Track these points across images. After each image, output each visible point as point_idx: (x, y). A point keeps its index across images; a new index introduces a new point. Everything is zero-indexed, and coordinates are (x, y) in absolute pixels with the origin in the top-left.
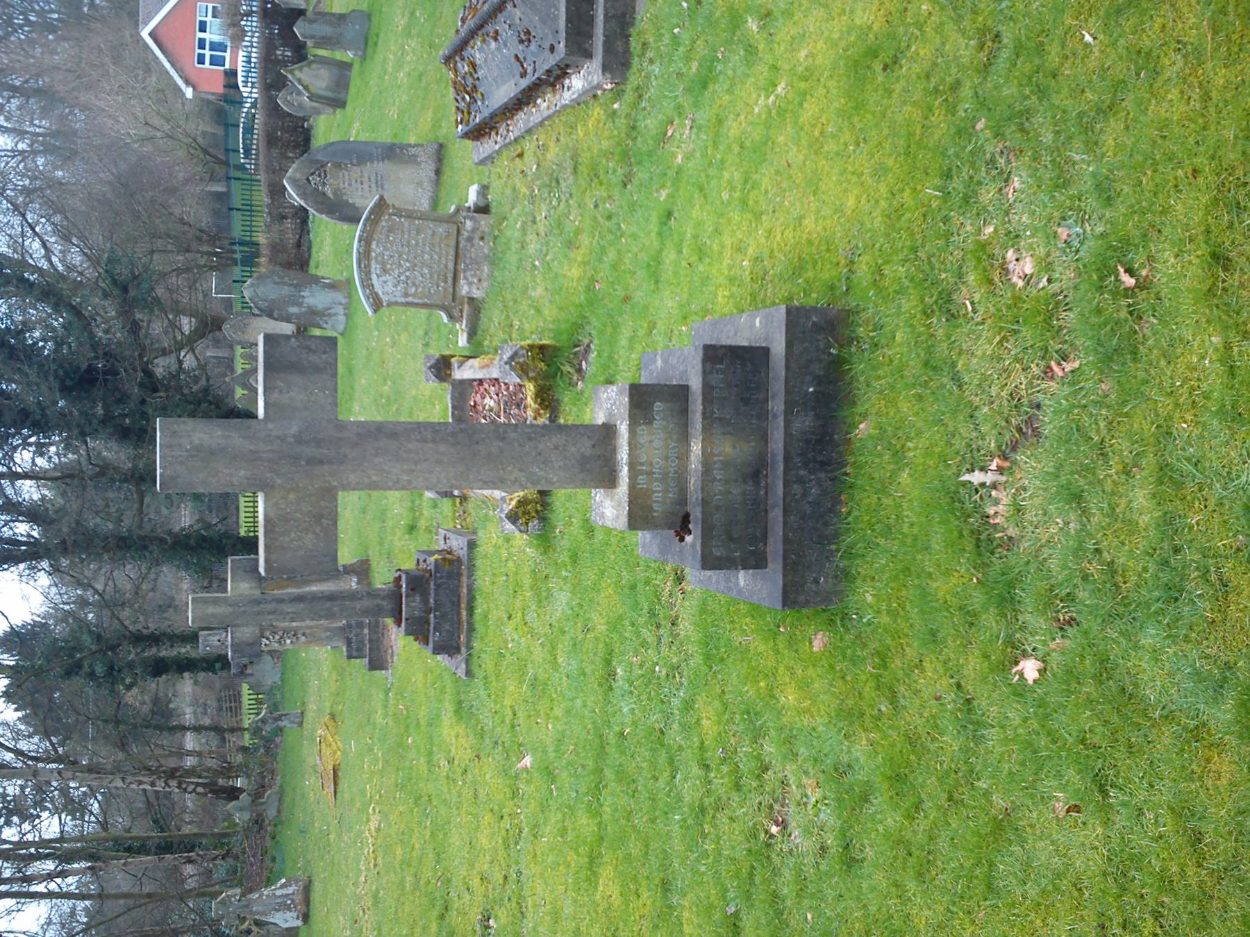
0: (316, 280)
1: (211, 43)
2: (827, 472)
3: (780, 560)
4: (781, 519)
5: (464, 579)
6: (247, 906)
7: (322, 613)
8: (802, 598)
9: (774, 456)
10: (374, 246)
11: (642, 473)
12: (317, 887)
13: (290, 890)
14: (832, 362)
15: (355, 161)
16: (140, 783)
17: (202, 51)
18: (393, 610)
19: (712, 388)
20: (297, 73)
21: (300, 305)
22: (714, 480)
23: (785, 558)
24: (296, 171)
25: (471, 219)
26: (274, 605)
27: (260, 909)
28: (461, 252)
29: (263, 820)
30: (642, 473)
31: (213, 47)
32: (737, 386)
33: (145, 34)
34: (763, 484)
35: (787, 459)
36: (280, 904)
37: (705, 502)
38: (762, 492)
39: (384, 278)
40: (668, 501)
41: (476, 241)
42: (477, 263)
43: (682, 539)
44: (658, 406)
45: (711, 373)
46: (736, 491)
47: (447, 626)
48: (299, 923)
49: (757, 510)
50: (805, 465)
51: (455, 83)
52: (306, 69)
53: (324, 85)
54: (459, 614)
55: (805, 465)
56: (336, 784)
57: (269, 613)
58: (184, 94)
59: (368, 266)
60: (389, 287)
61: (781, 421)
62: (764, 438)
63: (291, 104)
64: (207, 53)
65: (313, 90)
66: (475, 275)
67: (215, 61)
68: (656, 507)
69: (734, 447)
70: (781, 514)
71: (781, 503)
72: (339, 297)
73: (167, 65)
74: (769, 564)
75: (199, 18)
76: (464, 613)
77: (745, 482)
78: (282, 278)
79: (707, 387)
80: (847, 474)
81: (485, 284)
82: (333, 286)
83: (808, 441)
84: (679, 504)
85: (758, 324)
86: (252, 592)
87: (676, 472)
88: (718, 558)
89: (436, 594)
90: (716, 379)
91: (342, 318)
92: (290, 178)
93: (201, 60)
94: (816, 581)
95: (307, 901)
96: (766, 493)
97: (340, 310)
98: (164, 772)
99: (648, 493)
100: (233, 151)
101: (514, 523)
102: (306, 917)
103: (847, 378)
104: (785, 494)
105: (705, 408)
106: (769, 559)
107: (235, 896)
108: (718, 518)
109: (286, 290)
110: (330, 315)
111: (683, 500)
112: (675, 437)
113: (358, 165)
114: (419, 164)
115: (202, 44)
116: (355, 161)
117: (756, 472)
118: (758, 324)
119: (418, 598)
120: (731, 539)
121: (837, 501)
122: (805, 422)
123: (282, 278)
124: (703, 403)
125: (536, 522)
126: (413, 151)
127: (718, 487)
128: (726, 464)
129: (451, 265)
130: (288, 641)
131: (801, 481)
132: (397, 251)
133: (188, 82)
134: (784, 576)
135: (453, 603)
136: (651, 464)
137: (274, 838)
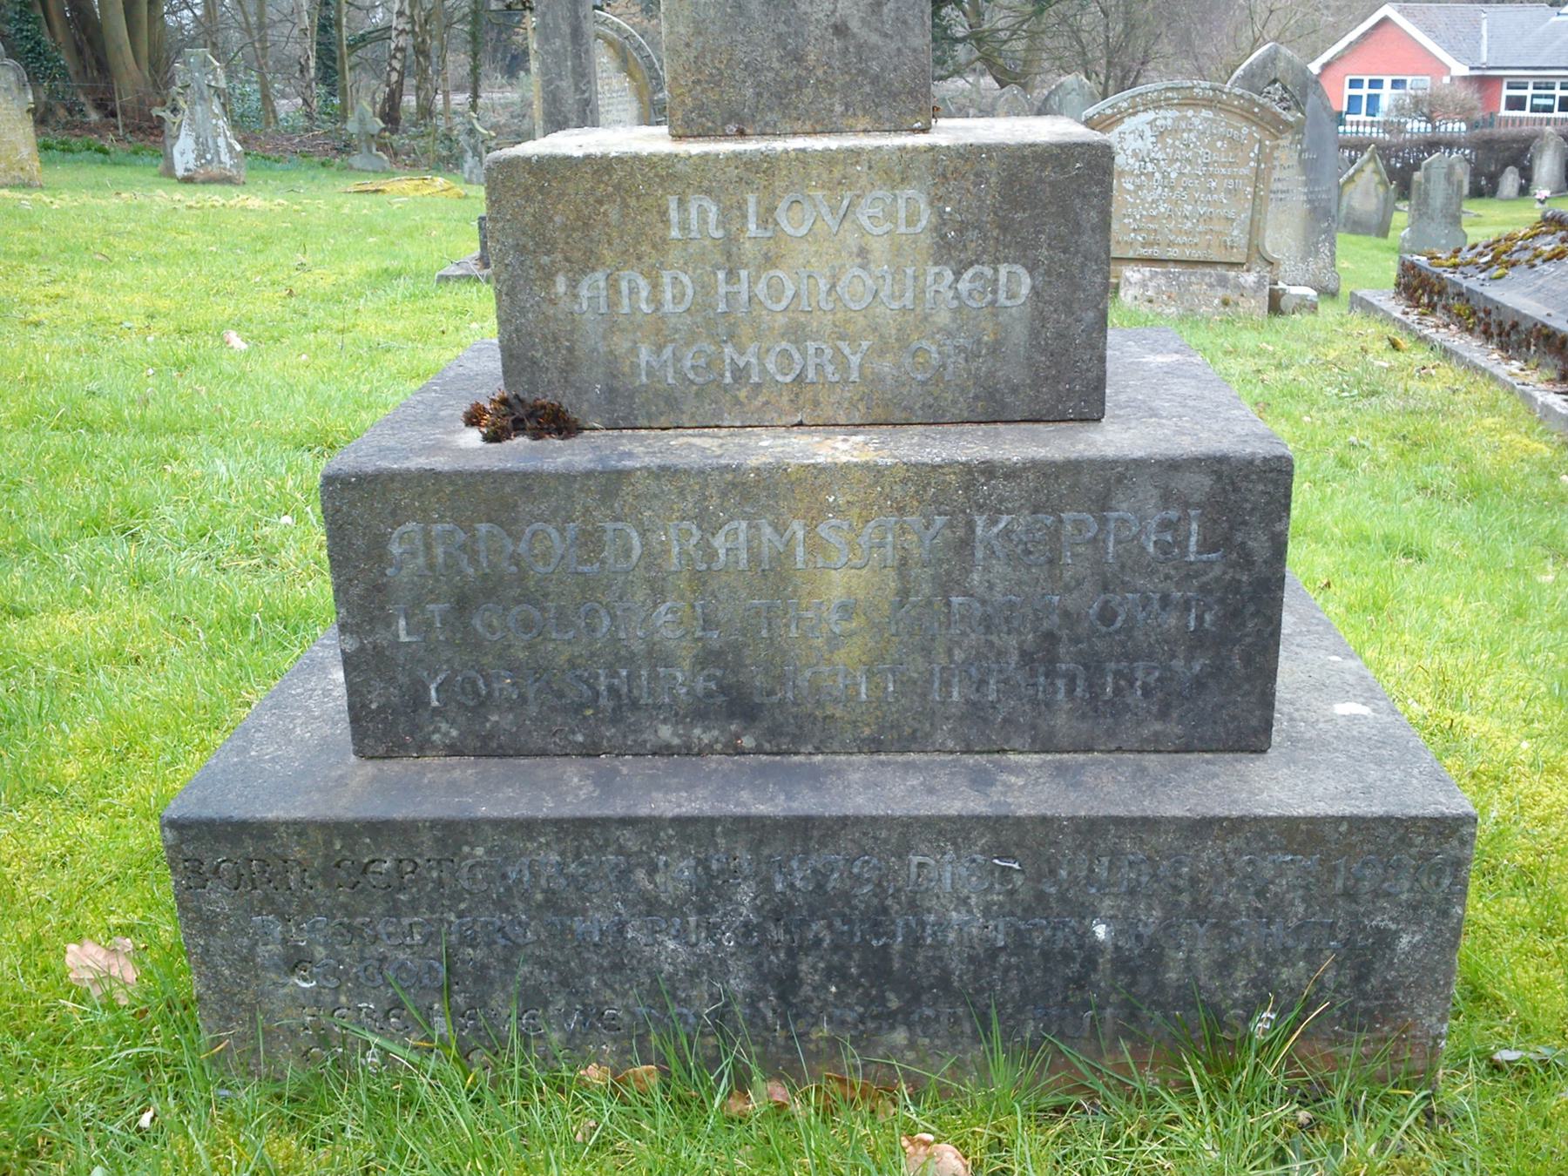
1: (1377, 96)
2: (753, 1000)
3: (376, 809)
4: (548, 808)
6: (202, 98)
7: (549, 19)
8: (218, 899)
9: (815, 777)
10: (1205, 113)
11: (732, 213)
13: (225, 158)
14: (1217, 1016)
15: (1306, 156)
17: (1366, 84)
19: (1102, 504)
20: (1371, 166)
22: (707, 523)
23: (378, 829)
24: (1289, 61)
25: (1259, 284)
27: (199, 116)
28: (1200, 270)
29: (348, 153)
30: (732, 213)
31: (1373, 100)
32: (1107, 616)
33: (1387, 10)
34: (701, 735)
35: (802, 829)
36: (205, 144)
37: (611, 482)
38: (666, 732)
39: (1148, 133)
40: (622, 344)
41: (1220, 292)
42: (1181, 295)
43: (473, 419)
44: (1017, 284)
45: (1167, 498)
46: (668, 623)
49: (595, 714)
50: (779, 911)
51: (1510, 238)
52: (1376, 178)
53: (1356, 204)
55: (779, 911)
59: (1169, 104)
60: (1132, 143)
61: (960, 802)
62: (889, 738)
64: (1364, 91)
65: (1348, 189)
66: (1159, 291)
67: (1354, 101)
68: (593, 286)
69: (846, 610)
70: (570, 809)
71: (617, 808)
73: (1353, 35)
74: (370, 768)
75: (1409, 79)
77: (707, 658)
79: (1115, 476)
80: (742, 1083)
81: (1145, 308)
83: (877, 919)
84: (611, 393)
85: (1344, 709)
87: (740, 374)
88: (377, 550)
90: (1140, 515)
92: (1277, 51)
93: (1355, 84)
94: (295, 962)
96: (664, 750)
98: (424, 41)
99: (644, 247)
102: (188, 180)
103: (1145, 1081)
104: (650, 826)
105: (1012, 473)
106: (393, 767)
107: (216, 80)
108: (547, 542)
111: (628, 411)
112: (886, 366)
113: (1301, 162)
114: (1304, 260)
115: (1375, 84)
116: (1306, 156)
117: (748, 706)
118: (1344, 709)
120: (463, 604)
121: (632, 1041)
122: (960, 904)
124: (1034, 465)
126: (1324, 249)
127: (676, 540)
128: (774, 574)
129: (1173, 253)
131: (709, 892)
132: (1197, 155)
134: (300, 828)
136: (769, 261)
137: (323, 164)
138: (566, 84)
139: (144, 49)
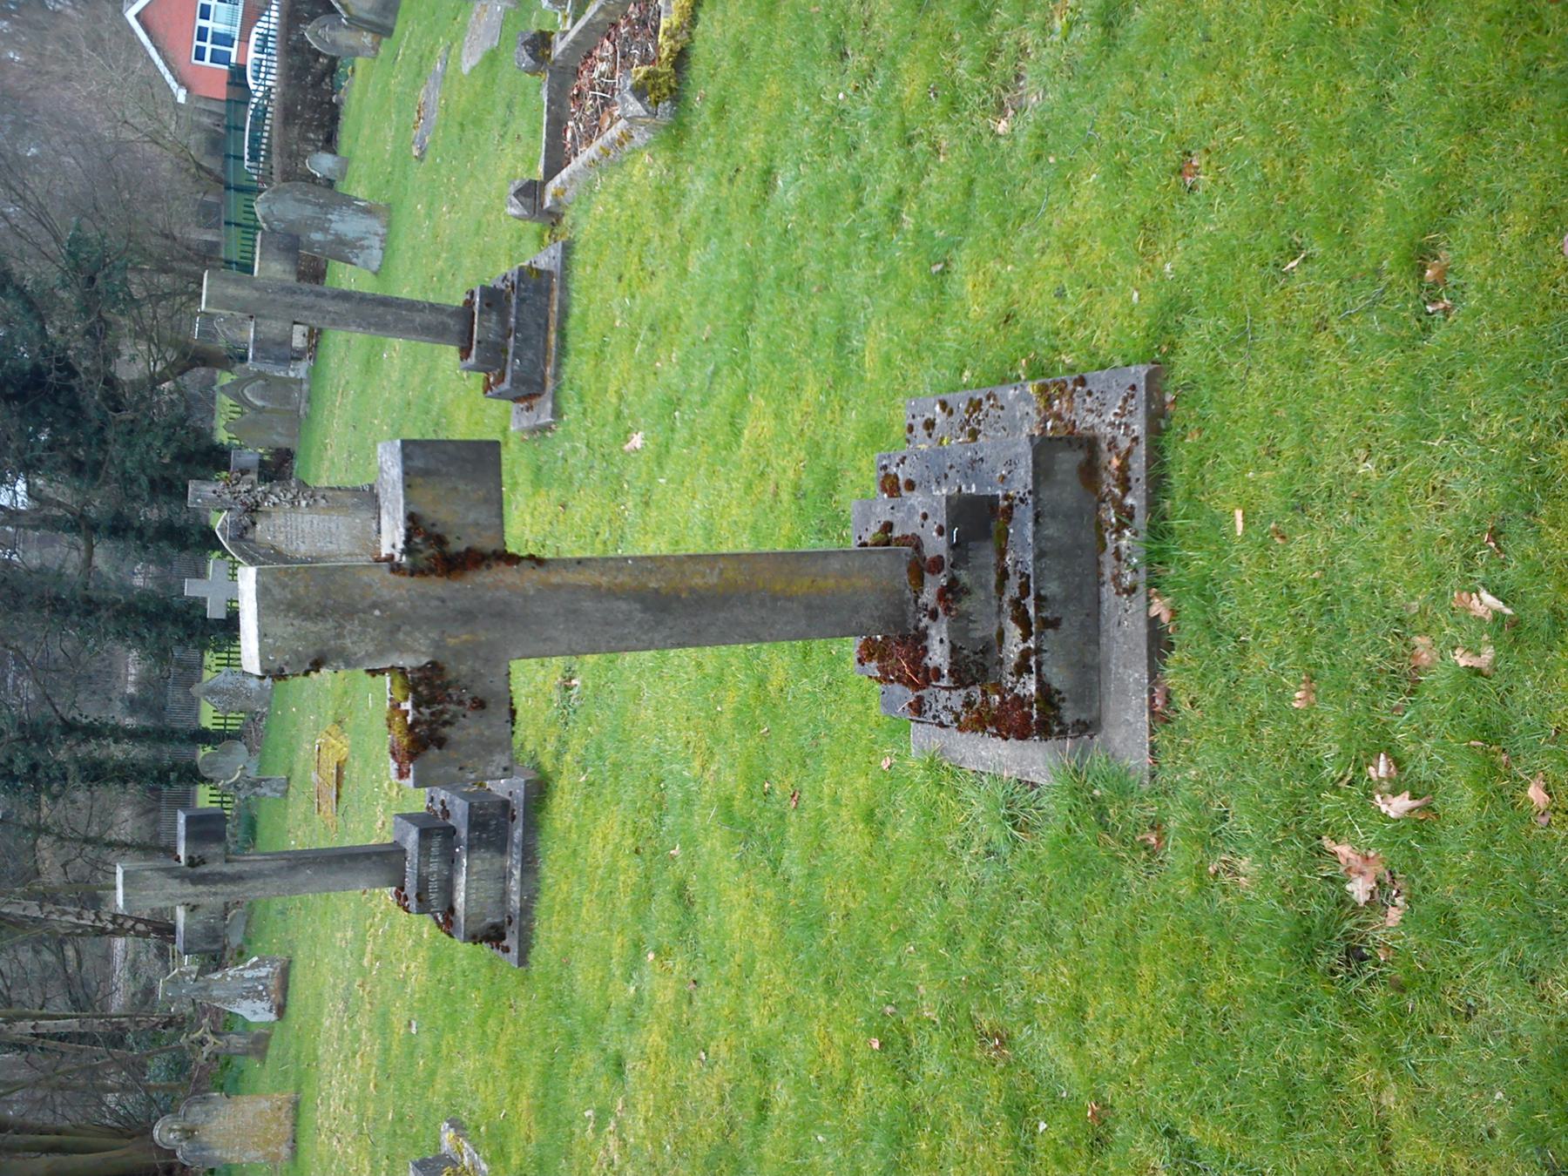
0: (348, 201)
1: (214, 34)
5: (556, 294)
6: (205, 989)
7: (372, 320)
12: (297, 973)
13: (263, 972)
16: (65, 913)
17: (201, 44)
18: (462, 332)
21: (325, 231)
26: (312, 298)
31: (219, 38)
33: (130, 15)
36: (249, 990)
47: (530, 354)
48: (272, 1017)
53: (367, 6)
54: (546, 340)
56: (339, 785)
57: (305, 308)
58: (174, 97)
63: (322, 41)
64: (208, 46)
65: (354, 12)
72: (375, 225)
76: (553, 337)
78: (306, 193)
82: (368, 211)
86: (286, 277)
89: (518, 310)
91: (377, 253)
93: (200, 54)
95: (284, 987)
97: (376, 242)
100: (235, 157)
101: (640, 99)
102: (281, 1010)
109: (309, 211)
110: (362, 248)
119: (494, 317)
123: (306, 193)
125: (668, 103)
130: (303, 503)
133: (181, 84)
135: (539, 325)
138: (418, 318)
139: (106, 1141)
